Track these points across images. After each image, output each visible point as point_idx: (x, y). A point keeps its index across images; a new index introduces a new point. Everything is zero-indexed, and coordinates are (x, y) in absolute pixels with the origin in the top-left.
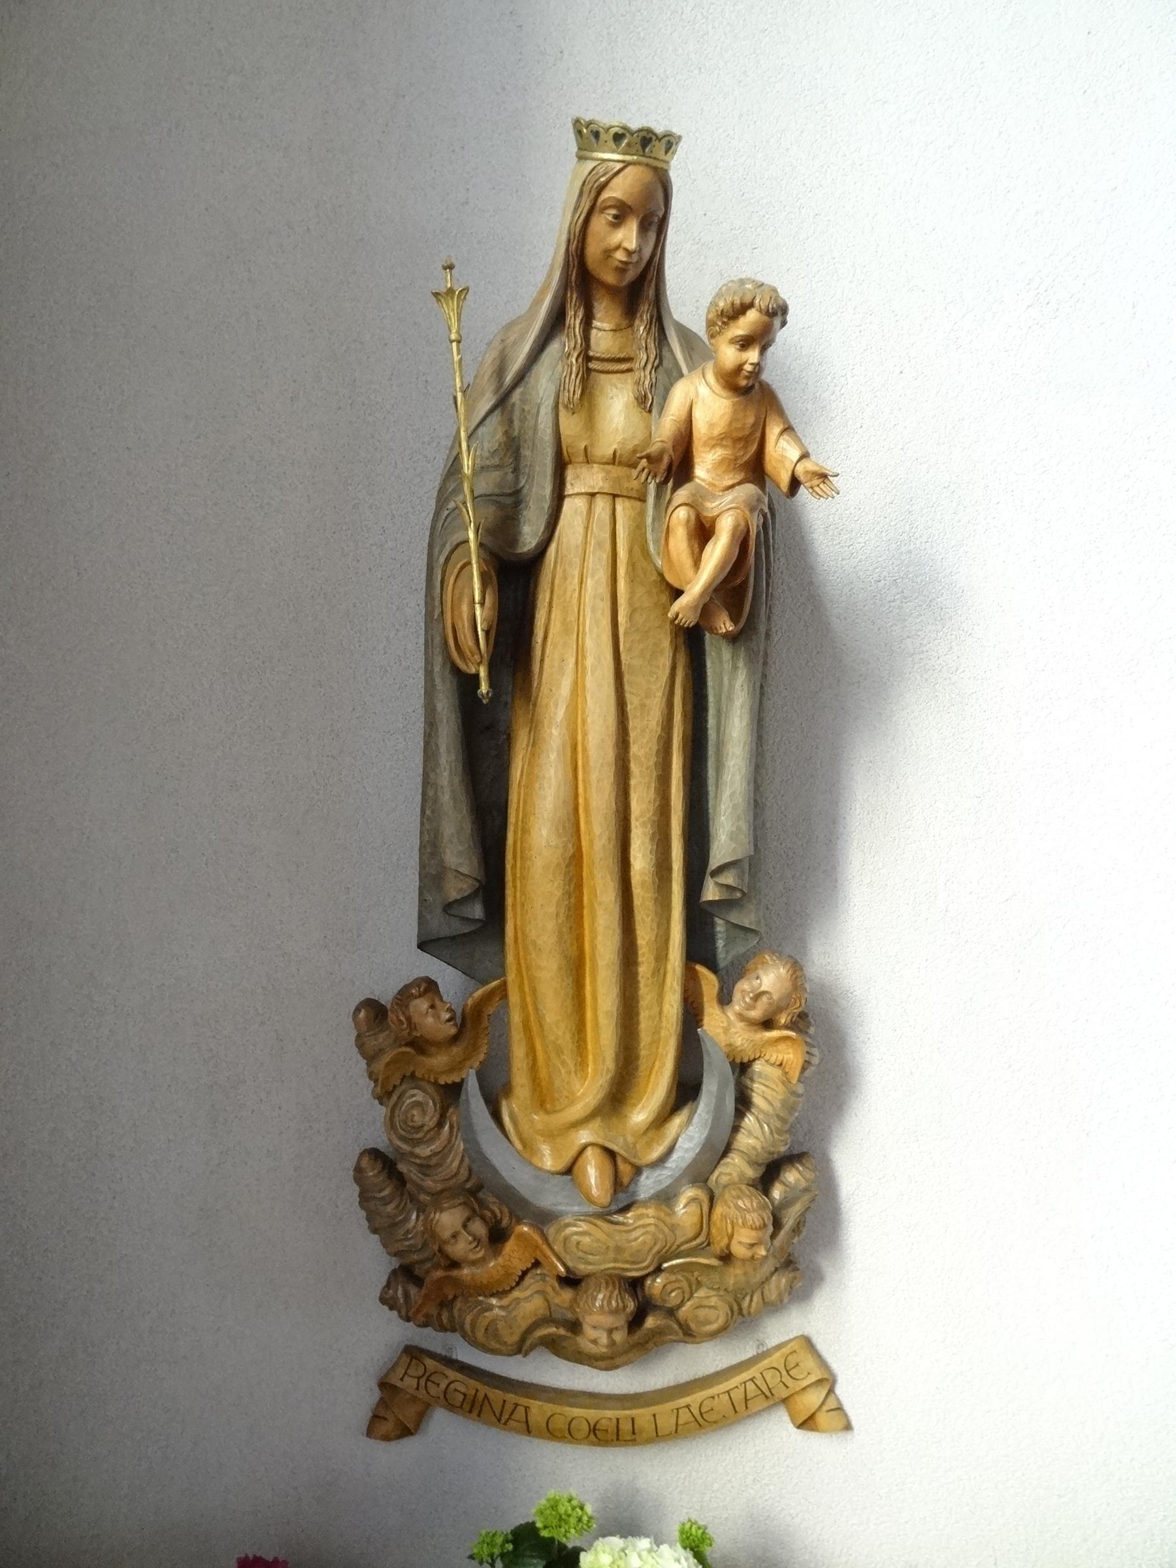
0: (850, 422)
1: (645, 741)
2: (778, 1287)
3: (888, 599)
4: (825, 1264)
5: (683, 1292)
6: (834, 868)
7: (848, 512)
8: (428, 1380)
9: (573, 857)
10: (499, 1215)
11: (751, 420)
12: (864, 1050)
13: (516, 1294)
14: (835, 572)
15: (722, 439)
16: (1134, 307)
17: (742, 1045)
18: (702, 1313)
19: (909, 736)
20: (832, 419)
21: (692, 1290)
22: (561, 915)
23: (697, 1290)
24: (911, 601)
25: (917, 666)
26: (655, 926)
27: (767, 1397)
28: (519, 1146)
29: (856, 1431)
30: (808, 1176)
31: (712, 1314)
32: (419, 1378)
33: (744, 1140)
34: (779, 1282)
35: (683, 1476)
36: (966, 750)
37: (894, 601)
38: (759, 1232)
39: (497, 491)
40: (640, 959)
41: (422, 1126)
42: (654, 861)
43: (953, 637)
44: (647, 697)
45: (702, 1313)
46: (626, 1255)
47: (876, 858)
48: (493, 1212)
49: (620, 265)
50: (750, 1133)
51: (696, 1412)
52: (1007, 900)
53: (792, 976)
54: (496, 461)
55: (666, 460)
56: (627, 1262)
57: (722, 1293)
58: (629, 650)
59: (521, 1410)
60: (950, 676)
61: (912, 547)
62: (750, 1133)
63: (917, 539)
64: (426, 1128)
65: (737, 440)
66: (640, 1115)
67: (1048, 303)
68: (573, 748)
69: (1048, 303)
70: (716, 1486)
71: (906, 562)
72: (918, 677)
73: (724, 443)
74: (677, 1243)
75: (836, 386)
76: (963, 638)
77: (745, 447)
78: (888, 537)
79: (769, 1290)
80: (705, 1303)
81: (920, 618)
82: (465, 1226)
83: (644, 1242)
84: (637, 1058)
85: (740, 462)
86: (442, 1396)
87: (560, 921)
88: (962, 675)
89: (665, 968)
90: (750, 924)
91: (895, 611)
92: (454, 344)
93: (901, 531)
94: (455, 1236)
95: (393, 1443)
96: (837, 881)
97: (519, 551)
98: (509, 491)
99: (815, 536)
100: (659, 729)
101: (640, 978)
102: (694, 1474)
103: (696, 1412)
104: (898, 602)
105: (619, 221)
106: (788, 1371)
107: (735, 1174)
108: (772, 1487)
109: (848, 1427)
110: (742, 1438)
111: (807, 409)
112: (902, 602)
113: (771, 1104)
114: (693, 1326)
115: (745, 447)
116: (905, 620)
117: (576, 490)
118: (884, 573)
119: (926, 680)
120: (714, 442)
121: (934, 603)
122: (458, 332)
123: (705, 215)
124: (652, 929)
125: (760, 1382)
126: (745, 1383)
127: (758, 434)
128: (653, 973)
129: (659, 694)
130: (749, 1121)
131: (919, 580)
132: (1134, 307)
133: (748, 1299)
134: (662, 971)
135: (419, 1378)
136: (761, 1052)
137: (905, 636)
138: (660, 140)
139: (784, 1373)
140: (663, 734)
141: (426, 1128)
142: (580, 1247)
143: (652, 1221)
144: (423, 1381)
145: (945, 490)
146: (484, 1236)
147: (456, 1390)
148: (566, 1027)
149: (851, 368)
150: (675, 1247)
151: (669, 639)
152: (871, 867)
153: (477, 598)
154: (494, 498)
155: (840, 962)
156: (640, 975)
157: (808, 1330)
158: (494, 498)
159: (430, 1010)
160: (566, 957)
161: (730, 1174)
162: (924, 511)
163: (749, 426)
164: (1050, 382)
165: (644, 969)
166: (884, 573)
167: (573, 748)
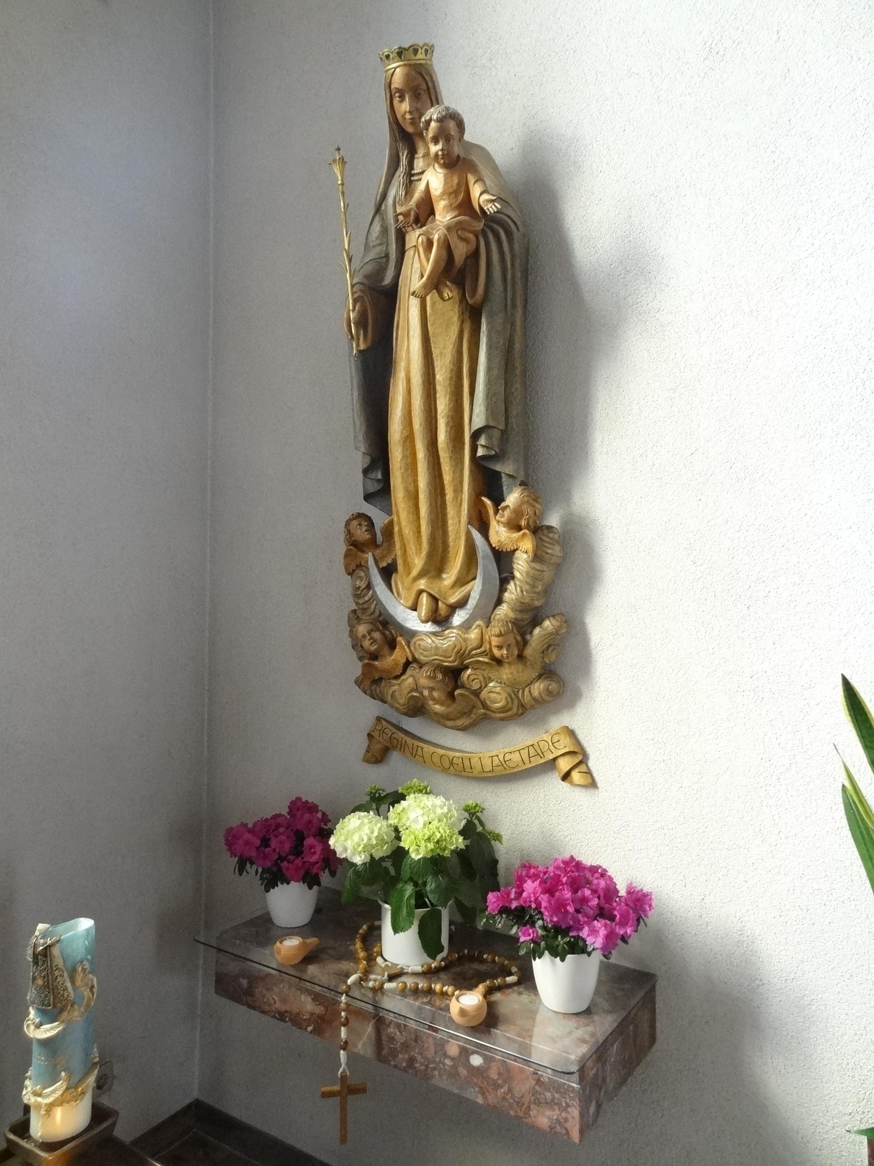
0: (595, 171)
1: (443, 372)
2: (538, 688)
3: (617, 274)
4: (583, 687)
5: (481, 682)
6: (586, 445)
7: (593, 226)
8: (383, 732)
9: (407, 437)
10: (395, 635)
11: (456, 181)
12: (604, 556)
13: (403, 677)
14: (586, 265)
15: (442, 196)
16: (778, 34)
17: (505, 540)
18: (493, 695)
19: (630, 357)
20: (584, 172)
21: (486, 681)
22: (402, 468)
23: (490, 683)
24: (631, 272)
25: (634, 312)
26: (451, 473)
27: (541, 758)
28: (396, 596)
29: (600, 790)
30: (554, 624)
31: (498, 697)
32: (380, 730)
33: (507, 596)
34: (540, 686)
35: (507, 804)
36: (665, 360)
37: (621, 275)
38: (499, 638)
39: (377, 257)
40: (447, 492)
41: (360, 587)
42: (448, 437)
43: (657, 289)
44: (444, 349)
45: (493, 695)
46: (440, 652)
47: (610, 436)
48: (391, 633)
49: (411, 121)
50: (511, 593)
51: (502, 759)
52: (692, 454)
53: (521, 495)
54: (379, 242)
55: (412, 213)
56: (441, 656)
57: (503, 685)
58: (433, 324)
59: (419, 749)
60: (655, 314)
61: (631, 239)
62: (511, 593)
63: (634, 232)
64: (361, 589)
65: (450, 194)
66: (450, 577)
67: (717, 53)
68: (408, 381)
69: (717, 53)
70: (524, 813)
71: (627, 249)
72: (636, 320)
73: (444, 197)
74: (469, 648)
75: (586, 151)
76: (663, 289)
77: (456, 197)
78: (617, 236)
79: (534, 688)
80: (494, 690)
81: (637, 282)
82: (369, 633)
83: (449, 645)
84: (449, 546)
85: (453, 206)
86: (389, 740)
87: (402, 471)
88: (662, 313)
89: (462, 498)
90: (509, 472)
91: (622, 280)
92: (340, 186)
93: (624, 230)
94: (364, 636)
95: (371, 765)
96: (587, 453)
97: (384, 284)
98: (383, 255)
99: (575, 246)
100: (451, 365)
101: (447, 503)
102: (513, 804)
103: (502, 759)
104: (623, 275)
105: (402, 98)
106: (553, 744)
107: (502, 614)
108: (553, 817)
109: (593, 784)
110: (538, 786)
111: (570, 171)
112: (625, 274)
113: (522, 575)
114: (488, 703)
115: (456, 197)
116: (627, 285)
117: (410, 246)
118: (615, 259)
119: (640, 320)
120: (439, 198)
121: (645, 270)
122: (342, 180)
123: (515, 76)
124: (450, 474)
125: (536, 747)
126: (528, 747)
127: (463, 189)
128: (453, 499)
129: (451, 347)
130: (511, 586)
131: (636, 257)
132: (778, 34)
133: (520, 692)
134: (459, 499)
135: (380, 730)
136: (517, 545)
137: (627, 295)
138: (408, 50)
139: (550, 744)
140: (454, 368)
141: (361, 589)
142: (421, 647)
143: (454, 635)
144: (381, 733)
145: (651, 197)
146: (379, 639)
147: (394, 738)
148: (410, 529)
149: (595, 137)
150: (467, 652)
151: (457, 316)
152: (607, 442)
153: (351, 308)
154: (376, 260)
155: (590, 502)
156: (447, 500)
157: (573, 726)
158: (376, 260)
159: (358, 526)
160: (407, 490)
161: (500, 614)
162: (638, 214)
163: (456, 184)
164: (719, 105)
165: (449, 496)
166: (615, 259)
167: (408, 381)
